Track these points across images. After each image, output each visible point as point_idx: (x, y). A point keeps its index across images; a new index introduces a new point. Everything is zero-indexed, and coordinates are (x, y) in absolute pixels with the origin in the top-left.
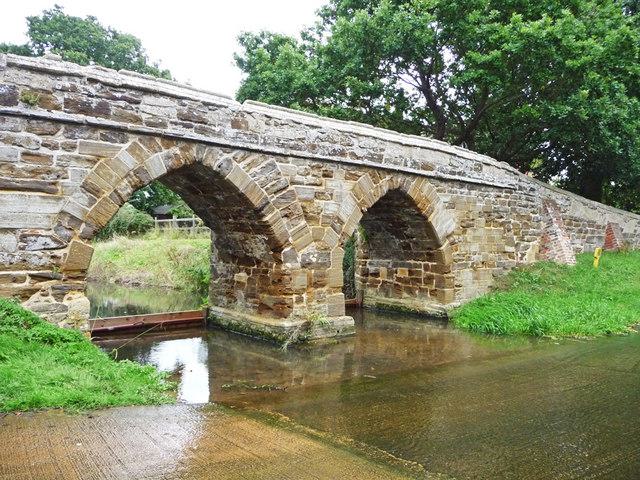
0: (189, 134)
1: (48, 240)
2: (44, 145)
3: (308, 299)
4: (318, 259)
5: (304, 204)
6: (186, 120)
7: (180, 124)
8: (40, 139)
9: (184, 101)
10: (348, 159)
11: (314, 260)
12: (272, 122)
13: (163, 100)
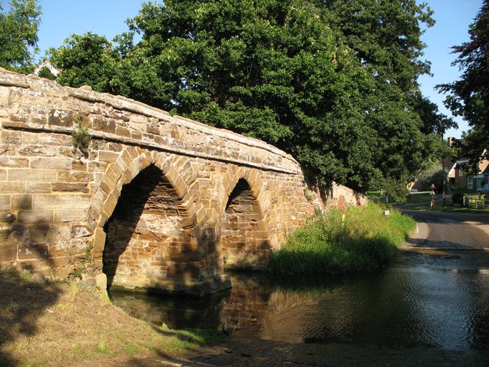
9: (151, 119)
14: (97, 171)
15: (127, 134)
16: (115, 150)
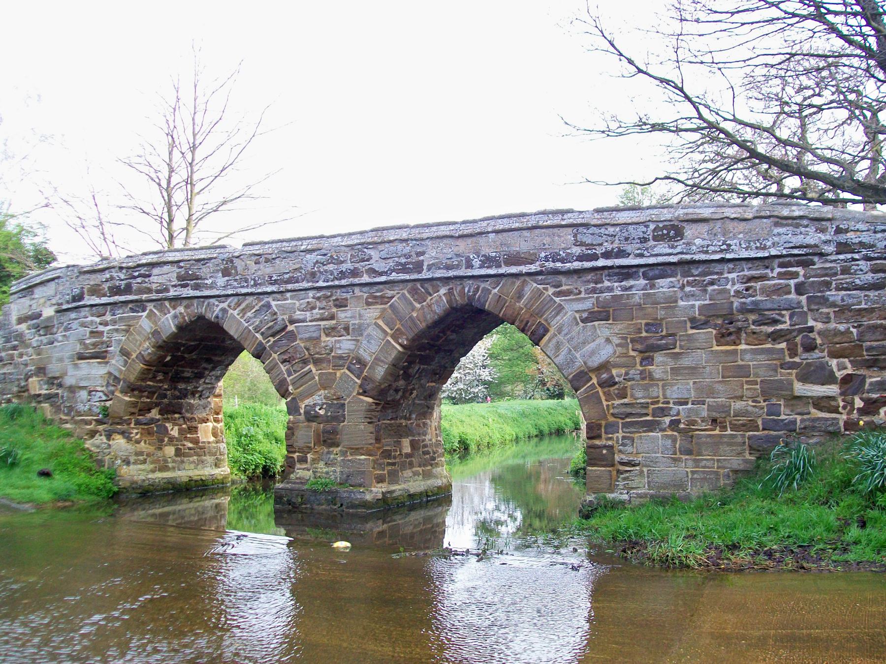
0: (189, 292)
1: (101, 394)
2: (101, 324)
3: (313, 460)
4: (326, 412)
5: (308, 344)
6: (184, 280)
7: (179, 285)
8: (98, 320)
9: (182, 264)
10: (366, 279)
11: (322, 412)
12: (262, 260)
13: (166, 268)
14: (117, 336)
15: (149, 291)
16: (138, 312)
